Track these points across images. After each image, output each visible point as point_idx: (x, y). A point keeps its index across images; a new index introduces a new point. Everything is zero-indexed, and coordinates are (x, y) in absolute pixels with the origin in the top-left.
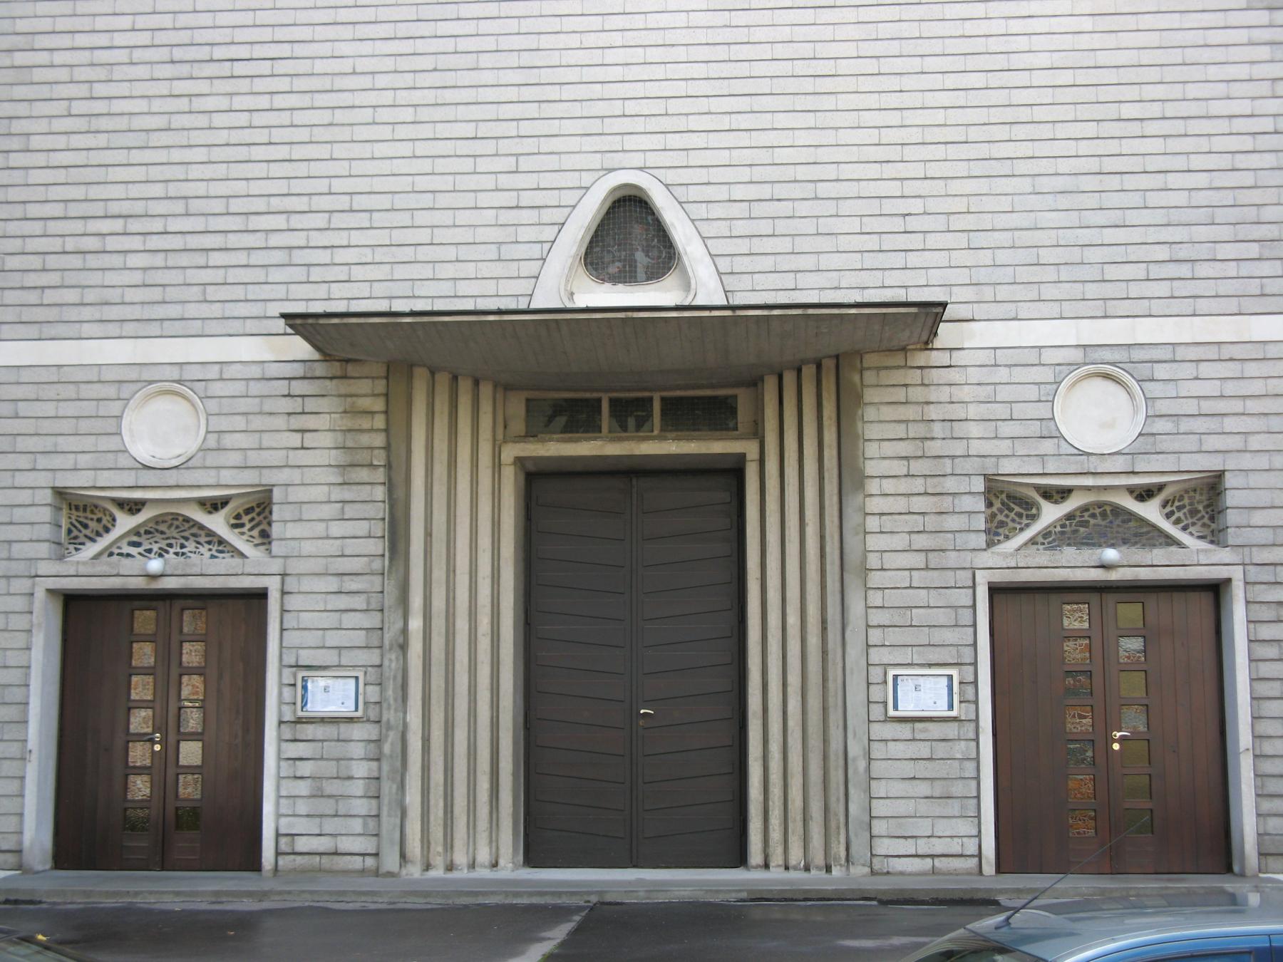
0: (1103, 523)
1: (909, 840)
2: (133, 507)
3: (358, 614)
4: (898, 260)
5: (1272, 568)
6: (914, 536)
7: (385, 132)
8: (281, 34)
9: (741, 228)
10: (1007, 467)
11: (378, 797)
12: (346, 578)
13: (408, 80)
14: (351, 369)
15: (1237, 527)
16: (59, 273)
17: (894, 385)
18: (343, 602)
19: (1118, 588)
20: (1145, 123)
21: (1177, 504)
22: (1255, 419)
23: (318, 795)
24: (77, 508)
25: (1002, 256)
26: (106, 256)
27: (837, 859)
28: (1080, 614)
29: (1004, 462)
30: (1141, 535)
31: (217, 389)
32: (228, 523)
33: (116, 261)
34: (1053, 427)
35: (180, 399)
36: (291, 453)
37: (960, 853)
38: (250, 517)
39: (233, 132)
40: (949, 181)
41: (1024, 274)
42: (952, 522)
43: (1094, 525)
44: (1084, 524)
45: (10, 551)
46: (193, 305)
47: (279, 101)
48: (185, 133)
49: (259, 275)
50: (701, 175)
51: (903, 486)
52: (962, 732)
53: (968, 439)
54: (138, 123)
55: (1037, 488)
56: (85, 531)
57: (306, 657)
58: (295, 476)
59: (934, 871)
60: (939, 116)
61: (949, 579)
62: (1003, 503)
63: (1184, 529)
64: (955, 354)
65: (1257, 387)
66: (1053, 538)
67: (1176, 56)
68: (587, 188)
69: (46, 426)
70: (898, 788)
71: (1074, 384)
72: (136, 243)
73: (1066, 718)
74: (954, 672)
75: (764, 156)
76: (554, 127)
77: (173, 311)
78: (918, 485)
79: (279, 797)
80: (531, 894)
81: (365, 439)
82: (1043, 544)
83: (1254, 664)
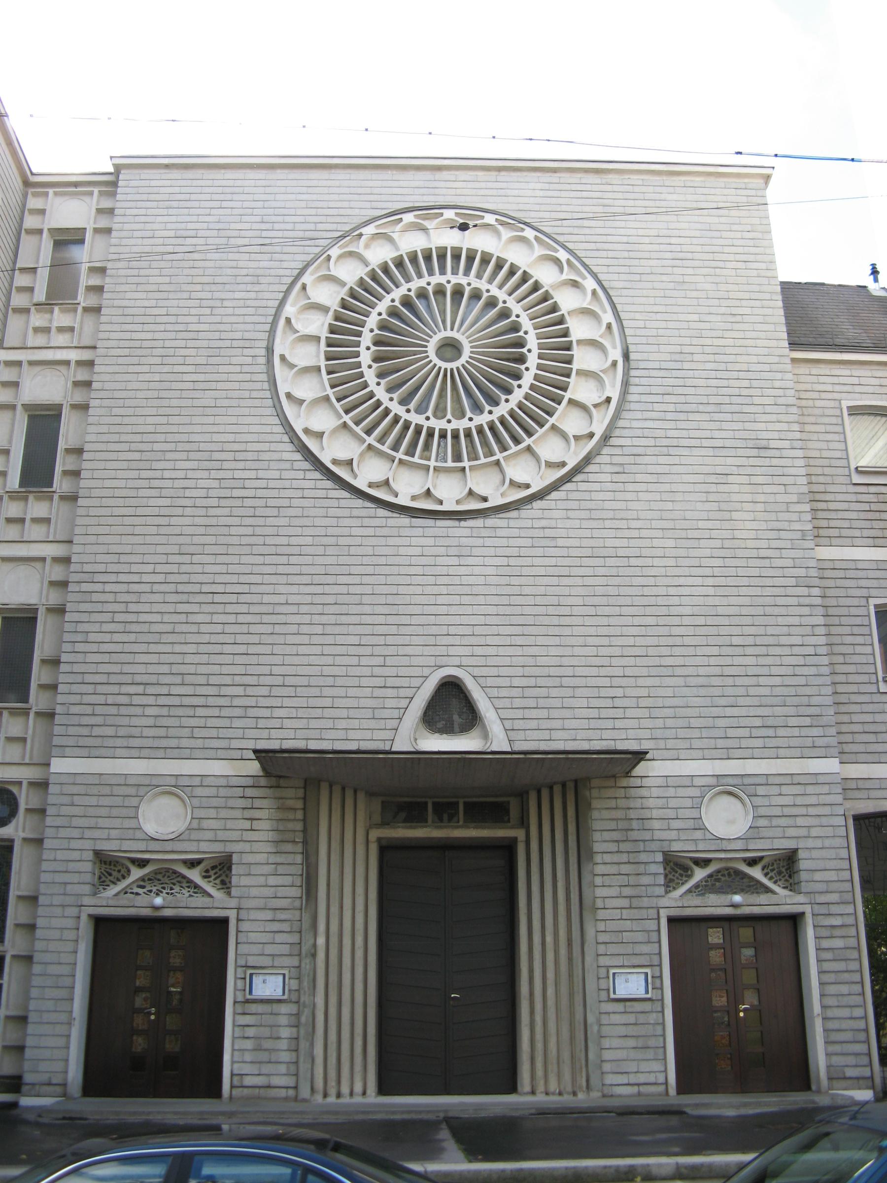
0: (730, 879)
1: (624, 1075)
2: (142, 863)
3: (285, 934)
4: (609, 724)
5: (827, 905)
6: (623, 888)
7: (305, 639)
8: (243, 579)
9: (517, 703)
10: (676, 847)
11: (296, 1050)
12: (277, 911)
13: (319, 609)
14: (282, 782)
16: (103, 717)
17: (609, 798)
18: (276, 926)
20: (746, 648)
21: (770, 868)
22: (813, 818)
23: (258, 1049)
24: (105, 863)
25: (670, 723)
26: (132, 708)
27: (580, 1087)
29: (673, 843)
30: (749, 886)
31: (199, 792)
32: (201, 874)
33: (139, 710)
34: (701, 823)
35: (173, 797)
36: (244, 832)
38: (214, 871)
39: (213, 636)
40: (638, 678)
41: (682, 733)
42: (645, 880)
44: (718, 880)
45: (65, 889)
46: (185, 739)
47: (241, 619)
48: (184, 635)
49: (226, 723)
50: (494, 671)
51: (616, 858)
54: (155, 628)
55: (691, 858)
56: (110, 878)
57: (252, 961)
58: (246, 847)
59: (639, 1094)
60: (631, 641)
61: (643, 914)
62: (672, 869)
63: (775, 882)
64: (644, 780)
65: (813, 800)
66: (701, 889)
67: (760, 611)
68: (427, 677)
69: (91, 811)
70: (616, 1043)
71: (711, 799)
72: (151, 700)
75: (530, 661)
76: (406, 640)
77: (173, 743)
78: (624, 858)
79: (233, 1050)
80: (403, 1112)
81: (290, 826)
83: (819, 963)
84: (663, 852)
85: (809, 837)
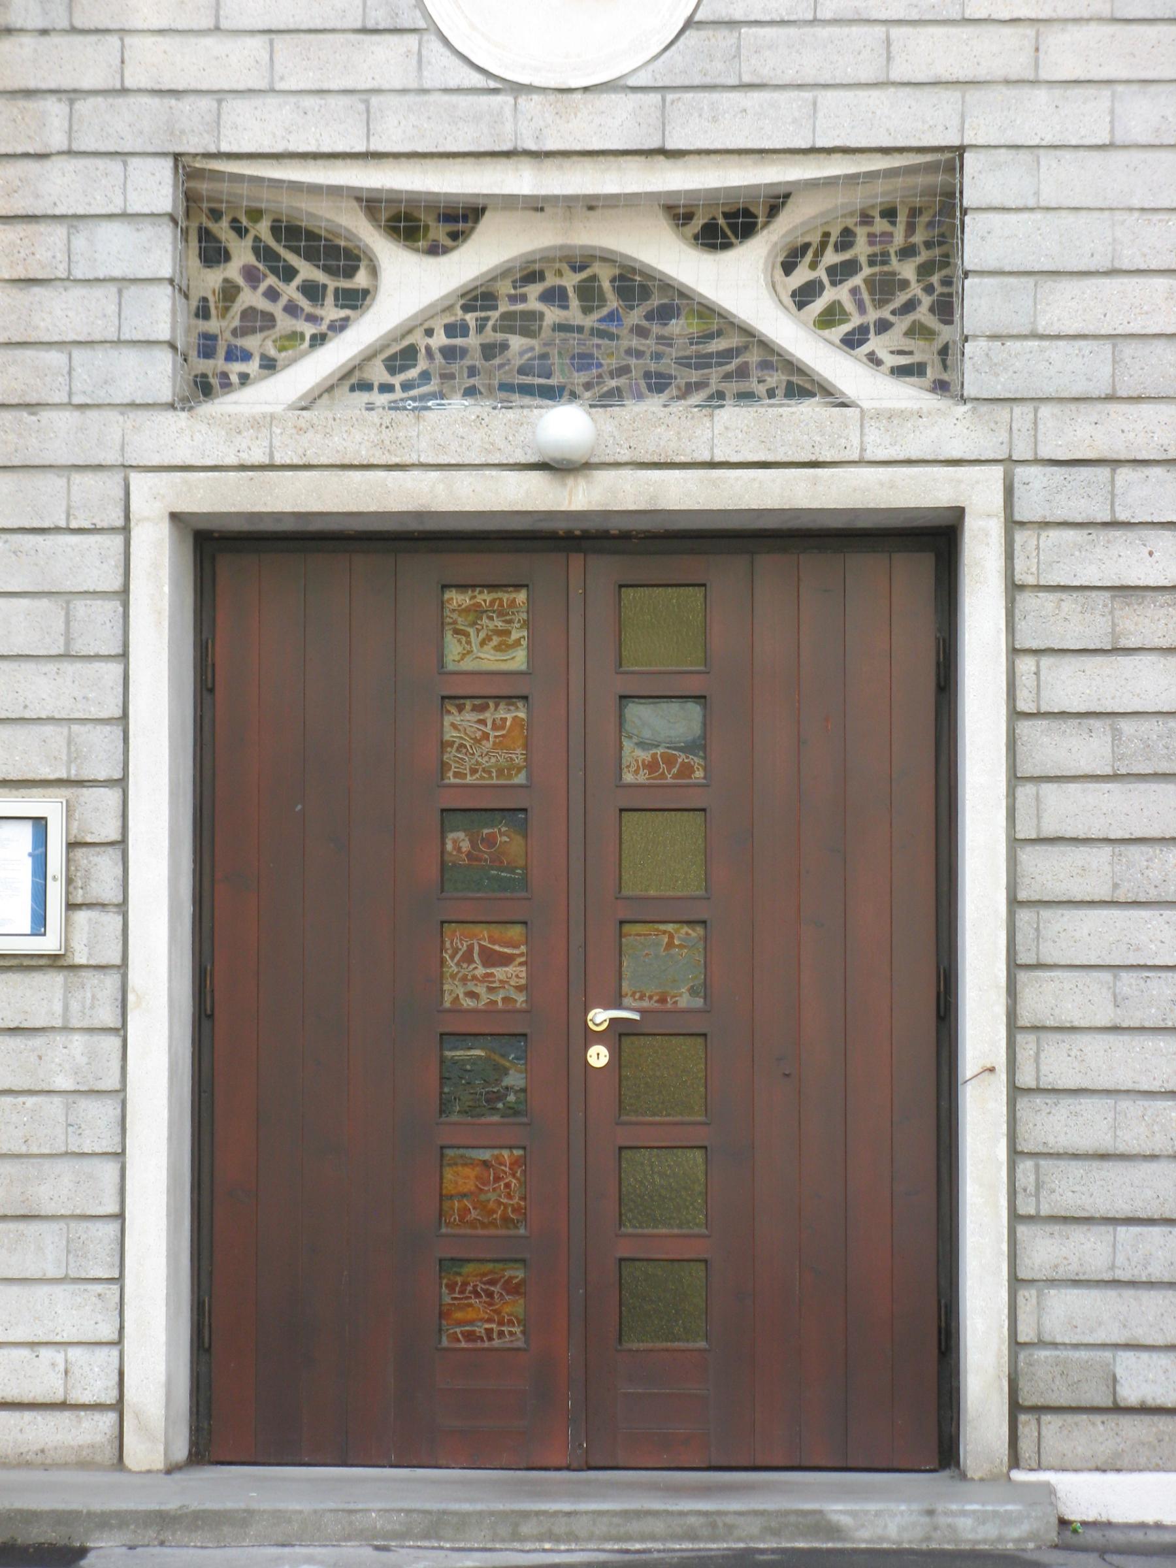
15: (994, 337)
19: (625, 536)
21: (831, 257)
28: (499, 624)
29: (236, 109)
37: (59, 1397)
43: (561, 327)
44: (527, 324)
52: (75, 1006)
53: (122, 32)
62: (262, 252)
63: (852, 341)
73: (442, 962)
74: (49, 806)
82: (386, 388)
84: (177, 156)
85: (1034, 83)
